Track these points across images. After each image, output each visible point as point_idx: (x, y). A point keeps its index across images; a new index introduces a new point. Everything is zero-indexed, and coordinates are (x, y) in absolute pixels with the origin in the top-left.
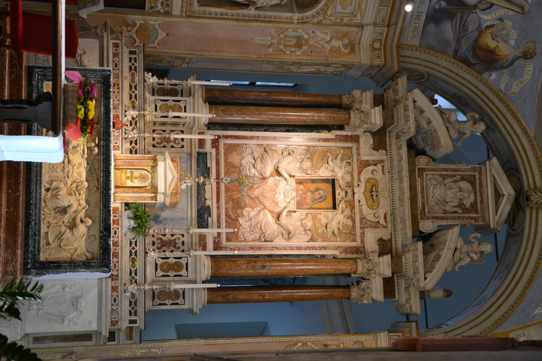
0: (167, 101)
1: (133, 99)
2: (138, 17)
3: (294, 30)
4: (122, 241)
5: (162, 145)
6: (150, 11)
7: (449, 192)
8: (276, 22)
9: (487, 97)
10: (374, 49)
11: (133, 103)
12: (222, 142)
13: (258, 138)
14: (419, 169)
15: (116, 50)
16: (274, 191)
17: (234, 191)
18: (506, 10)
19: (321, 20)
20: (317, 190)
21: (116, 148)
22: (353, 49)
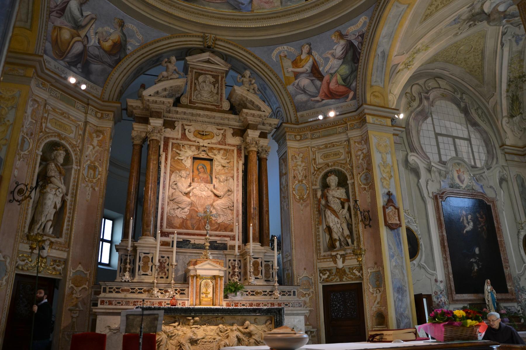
0: (139, 266)
1: (142, 291)
2: (67, 285)
3: (84, 170)
4: (249, 301)
5: (167, 272)
6: (62, 275)
7: (206, 89)
8: (78, 182)
9: (142, 54)
10: (102, 118)
11: (145, 291)
12: (165, 230)
13: (163, 204)
14: (190, 103)
15: (106, 303)
16: (200, 198)
17: (199, 224)
18: (91, 28)
20: (198, 169)
21: (184, 304)
22: (100, 132)
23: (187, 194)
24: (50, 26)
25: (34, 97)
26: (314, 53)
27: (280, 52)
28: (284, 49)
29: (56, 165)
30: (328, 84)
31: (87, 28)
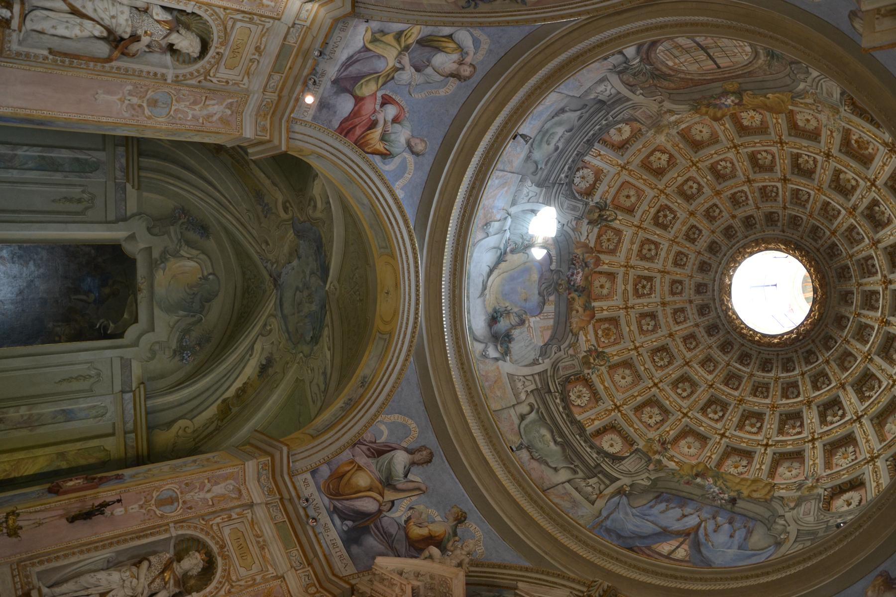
19: (229, 590)
24: (346, 455)
25: (242, 488)
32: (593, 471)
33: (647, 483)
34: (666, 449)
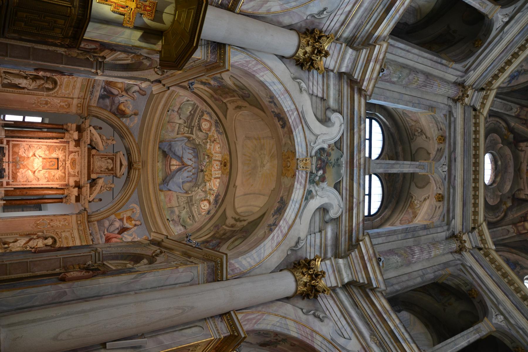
10: (78, 106)
12: (11, 143)
13: (27, 141)
16: (33, 162)
20: (51, 161)
23: (34, 155)
26: (136, 228)
27: (136, 208)
28: (138, 210)
29: (43, 84)
30: (116, 238)
31: (127, 96)
32: (190, 127)
33: (197, 143)
34: (213, 142)
